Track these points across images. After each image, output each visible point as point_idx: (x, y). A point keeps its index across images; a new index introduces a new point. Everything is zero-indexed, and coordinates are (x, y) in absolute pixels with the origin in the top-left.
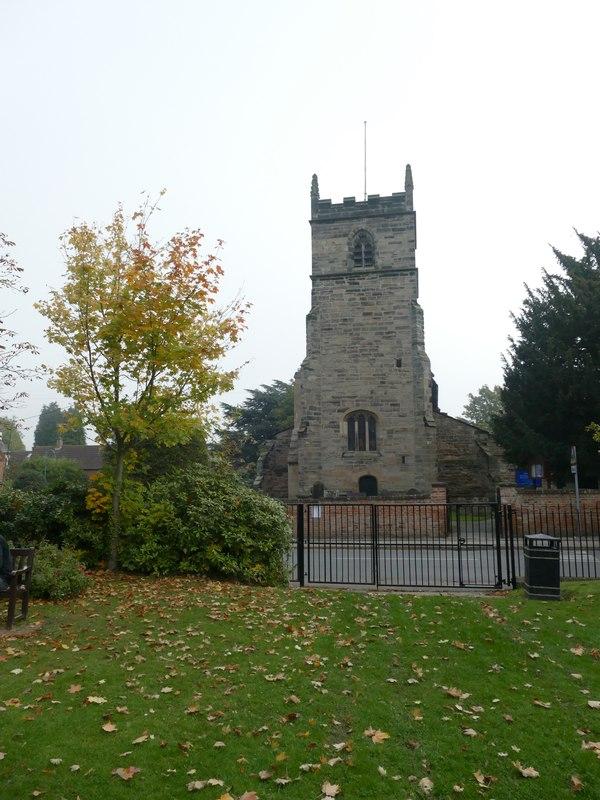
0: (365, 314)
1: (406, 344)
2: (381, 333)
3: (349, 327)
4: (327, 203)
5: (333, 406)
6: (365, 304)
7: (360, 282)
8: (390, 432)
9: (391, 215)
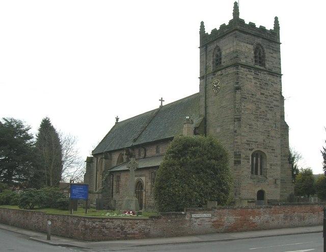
0: (262, 94)
1: (278, 117)
2: (268, 107)
3: (255, 100)
4: (242, 21)
5: (246, 146)
6: (262, 88)
7: (259, 74)
8: (271, 165)
9: (265, 43)
